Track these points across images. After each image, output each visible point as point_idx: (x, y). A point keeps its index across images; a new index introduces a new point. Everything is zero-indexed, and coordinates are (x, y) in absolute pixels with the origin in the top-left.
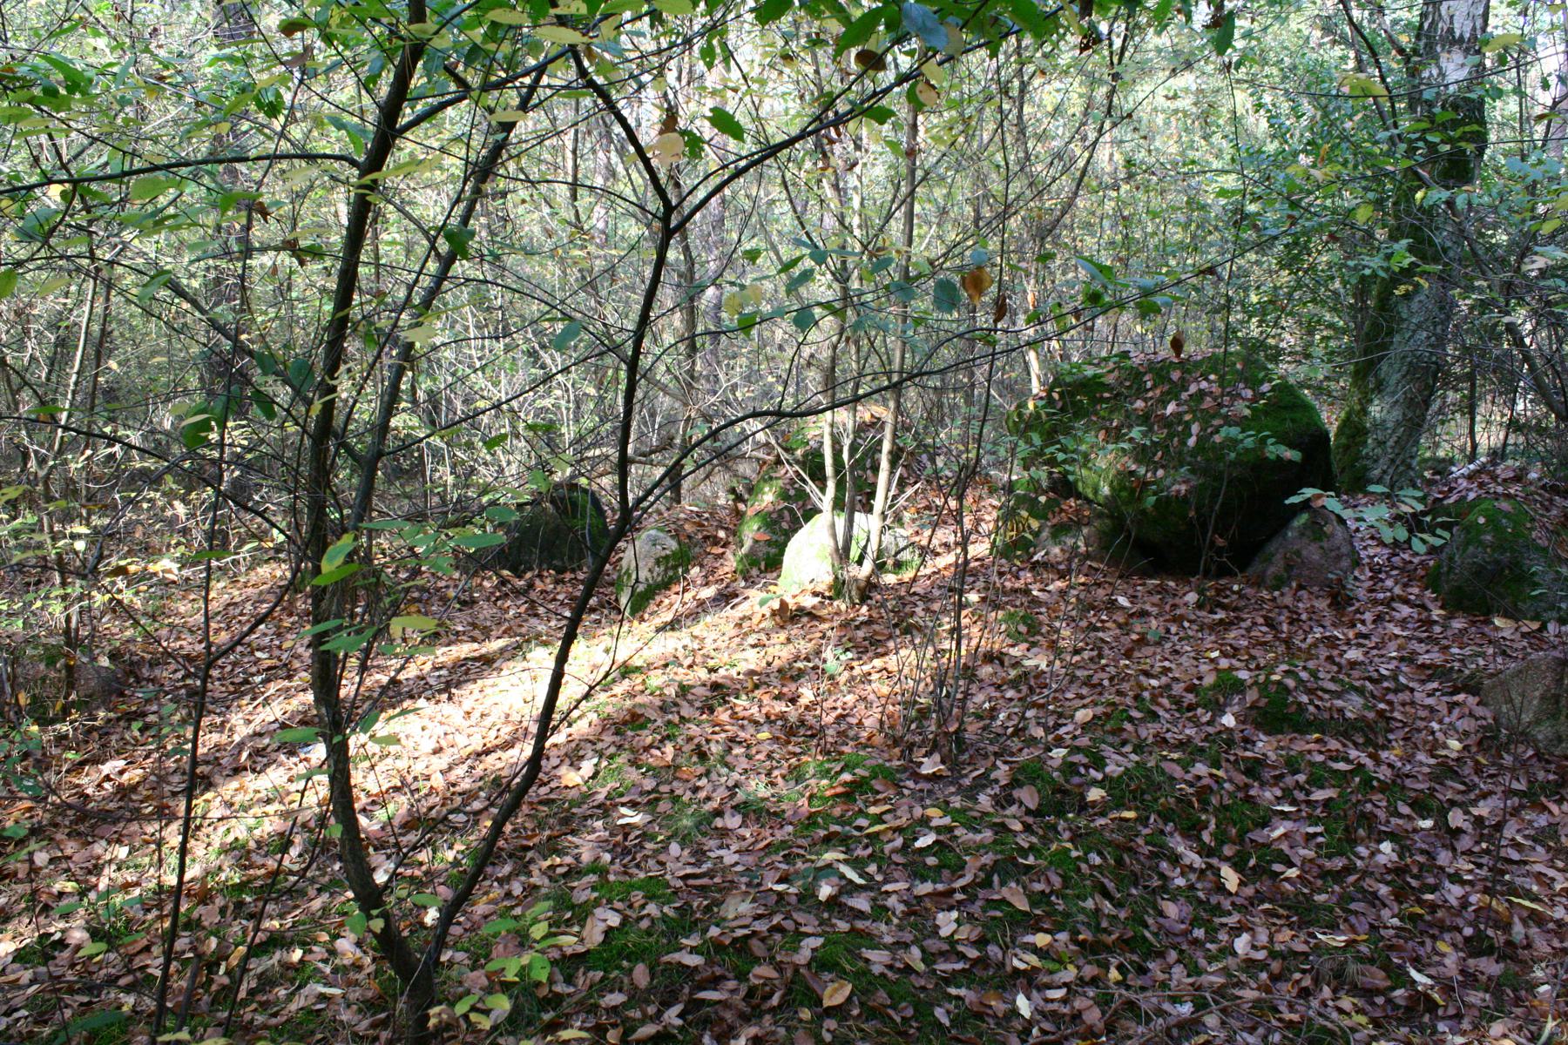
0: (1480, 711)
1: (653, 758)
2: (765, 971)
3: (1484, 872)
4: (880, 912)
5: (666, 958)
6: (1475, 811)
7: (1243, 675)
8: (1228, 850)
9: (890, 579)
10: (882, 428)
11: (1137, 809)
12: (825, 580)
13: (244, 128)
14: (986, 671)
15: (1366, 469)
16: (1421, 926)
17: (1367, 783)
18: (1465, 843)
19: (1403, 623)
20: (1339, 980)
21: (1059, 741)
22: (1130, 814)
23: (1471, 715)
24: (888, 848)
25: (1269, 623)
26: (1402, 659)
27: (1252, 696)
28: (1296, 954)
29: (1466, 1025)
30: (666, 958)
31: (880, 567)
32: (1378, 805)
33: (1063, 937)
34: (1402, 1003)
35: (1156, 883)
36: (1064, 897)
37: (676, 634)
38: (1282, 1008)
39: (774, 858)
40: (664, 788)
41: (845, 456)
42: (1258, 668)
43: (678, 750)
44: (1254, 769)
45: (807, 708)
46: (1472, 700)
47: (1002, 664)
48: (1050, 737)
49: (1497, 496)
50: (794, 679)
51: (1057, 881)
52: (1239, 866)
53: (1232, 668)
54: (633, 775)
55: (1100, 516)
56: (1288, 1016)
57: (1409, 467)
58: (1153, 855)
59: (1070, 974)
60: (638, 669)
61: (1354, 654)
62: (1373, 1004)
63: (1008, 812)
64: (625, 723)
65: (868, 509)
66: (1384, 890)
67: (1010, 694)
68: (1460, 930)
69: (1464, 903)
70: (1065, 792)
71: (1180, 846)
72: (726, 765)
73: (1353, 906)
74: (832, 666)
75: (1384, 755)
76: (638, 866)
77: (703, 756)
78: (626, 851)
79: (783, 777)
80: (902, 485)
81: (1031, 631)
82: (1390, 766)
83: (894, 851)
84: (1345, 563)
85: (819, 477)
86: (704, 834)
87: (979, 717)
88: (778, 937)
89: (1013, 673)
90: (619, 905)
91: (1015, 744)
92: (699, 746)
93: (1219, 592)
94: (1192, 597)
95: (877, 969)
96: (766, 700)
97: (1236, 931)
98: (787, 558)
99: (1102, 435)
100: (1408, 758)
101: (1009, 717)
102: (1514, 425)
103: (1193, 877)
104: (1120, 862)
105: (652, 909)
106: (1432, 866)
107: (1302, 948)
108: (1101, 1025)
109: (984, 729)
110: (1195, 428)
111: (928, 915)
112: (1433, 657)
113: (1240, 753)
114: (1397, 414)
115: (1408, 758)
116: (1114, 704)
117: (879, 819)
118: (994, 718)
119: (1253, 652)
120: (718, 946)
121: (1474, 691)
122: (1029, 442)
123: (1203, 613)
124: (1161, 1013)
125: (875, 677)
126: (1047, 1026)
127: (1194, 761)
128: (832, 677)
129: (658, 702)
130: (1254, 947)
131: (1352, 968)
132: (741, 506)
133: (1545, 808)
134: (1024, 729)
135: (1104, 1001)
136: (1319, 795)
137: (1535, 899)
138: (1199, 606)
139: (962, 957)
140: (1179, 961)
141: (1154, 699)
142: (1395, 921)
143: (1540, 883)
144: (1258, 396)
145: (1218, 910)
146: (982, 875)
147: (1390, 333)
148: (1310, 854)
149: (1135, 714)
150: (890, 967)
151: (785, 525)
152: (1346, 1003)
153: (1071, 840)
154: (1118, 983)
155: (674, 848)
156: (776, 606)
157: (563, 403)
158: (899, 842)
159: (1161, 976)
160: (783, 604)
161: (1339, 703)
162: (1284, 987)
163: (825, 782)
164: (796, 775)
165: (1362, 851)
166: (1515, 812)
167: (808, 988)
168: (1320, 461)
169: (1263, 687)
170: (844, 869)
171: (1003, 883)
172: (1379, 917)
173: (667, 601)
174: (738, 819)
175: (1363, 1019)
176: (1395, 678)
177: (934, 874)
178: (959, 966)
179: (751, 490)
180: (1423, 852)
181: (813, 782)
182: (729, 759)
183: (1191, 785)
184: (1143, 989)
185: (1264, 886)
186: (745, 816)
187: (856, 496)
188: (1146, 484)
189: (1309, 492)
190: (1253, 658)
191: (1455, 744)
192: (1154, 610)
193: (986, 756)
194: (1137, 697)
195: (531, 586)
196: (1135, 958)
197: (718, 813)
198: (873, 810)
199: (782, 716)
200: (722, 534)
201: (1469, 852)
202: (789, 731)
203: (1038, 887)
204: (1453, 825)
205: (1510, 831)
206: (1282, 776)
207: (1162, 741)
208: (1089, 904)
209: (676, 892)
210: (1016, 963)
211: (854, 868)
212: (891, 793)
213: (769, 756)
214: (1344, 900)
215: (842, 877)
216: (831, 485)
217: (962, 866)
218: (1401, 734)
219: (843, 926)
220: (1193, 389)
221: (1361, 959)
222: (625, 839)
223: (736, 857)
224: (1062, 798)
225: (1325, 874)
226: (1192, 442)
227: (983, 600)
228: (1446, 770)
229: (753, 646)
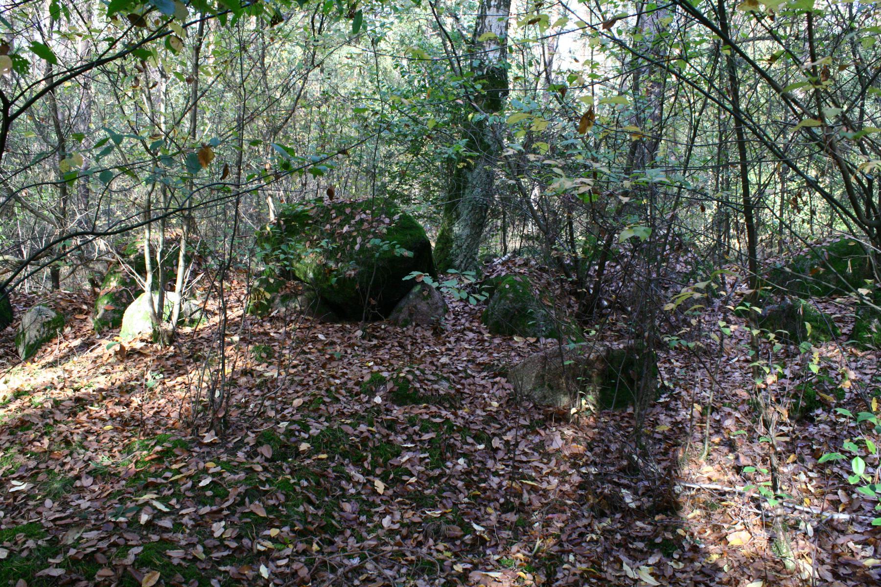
0: (507, 386)
1: (36, 447)
2: (106, 572)
3: (509, 469)
4: (178, 526)
5: (40, 573)
6: (505, 438)
7: (385, 374)
8: (378, 471)
9: (188, 330)
10: (179, 242)
11: (327, 453)
12: (148, 332)
14: (243, 380)
15: (452, 261)
16: (479, 500)
17: (451, 428)
18: (500, 455)
19: (470, 342)
20: (438, 535)
21: (284, 418)
22: (324, 456)
23: (503, 388)
24: (183, 488)
25: (401, 345)
26: (469, 361)
27: (390, 385)
28: (415, 523)
29: (500, 549)
30: (40, 573)
31: (181, 323)
32: (456, 440)
33: (286, 529)
34: (469, 542)
35: (339, 493)
36: (286, 506)
37: (54, 369)
38: (408, 554)
39: (113, 501)
40: (43, 466)
41: (158, 258)
42: (393, 370)
43: (52, 441)
44: (391, 425)
45: (136, 409)
46: (503, 380)
47: (252, 376)
48: (278, 416)
49: (516, 274)
50: (128, 392)
51: (282, 498)
52: (384, 479)
53: (380, 371)
54: (21, 459)
55: (308, 289)
56: (411, 558)
57: (474, 259)
58: (337, 478)
59: (288, 551)
60: (27, 393)
61: (444, 360)
62: (455, 545)
63: (255, 460)
64: (17, 427)
65: (173, 289)
66: (460, 484)
67: (257, 393)
68: (498, 500)
69: (500, 486)
70: (287, 447)
71: (353, 471)
72: (84, 447)
73: (445, 494)
74: (151, 382)
75: (460, 412)
76: (23, 517)
77: (67, 443)
78: (15, 508)
79: (120, 451)
80: (194, 274)
81: (269, 355)
82: (463, 418)
83: (187, 490)
84: (441, 311)
85: (142, 271)
86: (69, 492)
87: (238, 407)
88: (114, 550)
89: (258, 381)
90: (7, 544)
91: (259, 421)
92: (66, 437)
93: (374, 329)
94: (359, 333)
95: (175, 562)
96: (110, 406)
97: (383, 515)
98: (124, 320)
99: (308, 244)
100: (472, 413)
101: (255, 406)
102: (528, 238)
103: (359, 488)
104: (318, 484)
105: (31, 543)
106: (484, 469)
107: (418, 520)
108: (308, 577)
109: (241, 414)
110: (359, 240)
111: (208, 525)
112: (483, 359)
113: (384, 417)
114: (467, 231)
115: (472, 413)
116: (315, 395)
117: (178, 471)
118: (247, 407)
119: (392, 361)
120: (74, 561)
121: (503, 374)
122: (264, 249)
123: (365, 342)
124: (341, 565)
125: (178, 387)
126: (277, 581)
127: (359, 424)
128: (151, 389)
129: (39, 412)
130: (393, 523)
131: (444, 527)
132: (97, 290)
133: (538, 433)
134: (264, 412)
135: (309, 564)
136: (426, 437)
137: (534, 480)
138: (363, 337)
139: (227, 547)
140: (351, 535)
141: (337, 391)
142: (466, 500)
143: (536, 471)
144: (392, 221)
145: (374, 505)
146: (239, 498)
147: (465, 188)
148: (422, 469)
149: (327, 400)
150: (184, 559)
151: (124, 300)
152: (441, 547)
153: (291, 474)
154: (317, 552)
155: (48, 503)
156: (118, 349)
158: (190, 484)
159: (342, 545)
160: (122, 347)
161: (436, 386)
162: (409, 542)
163: (145, 452)
164: (128, 449)
165: (449, 464)
166: (524, 437)
167: (133, 579)
168: (423, 257)
169: (395, 380)
170: (155, 503)
171: (251, 502)
172: (458, 499)
173: (49, 349)
174: (90, 480)
175: (449, 554)
176: (465, 371)
177: (211, 500)
178: (225, 553)
179: (104, 279)
180: (479, 462)
181: (138, 453)
182: (85, 443)
183: (357, 437)
184: (332, 553)
185: (398, 488)
186: (95, 478)
187: (165, 281)
188: (331, 271)
189: (415, 274)
190: (392, 364)
191: (495, 404)
192: (339, 341)
193: (242, 430)
194: (328, 390)
196: (327, 536)
197: (78, 477)
198: (174, 467)
199: (120, 415)
200: (85, 307)
201: (502, 460)
202: (123, 423)
203: (271, 502)
204: (494, 446)
205: (521, 447)
206: (406, 428)
207: (341, 414)
208: (301, 509)
209: (48, 530)
210: (259, 547)
211: (162, 503)
212: (185, 455)
213: (111, 440)
214: (440, 491)
215: (155, 508)
216: (149, 276)
217: (227, 494)
218: (468, 400)
219: (155, 538)
220: (357, 218)
221: (448, 522)
222: (15, 500)
223: (89, 504)
224: (286, 450)
225: (430, 479)
226: (357, 247)
227: (241, 339)
228: (491, 418)
229: (103, 374)
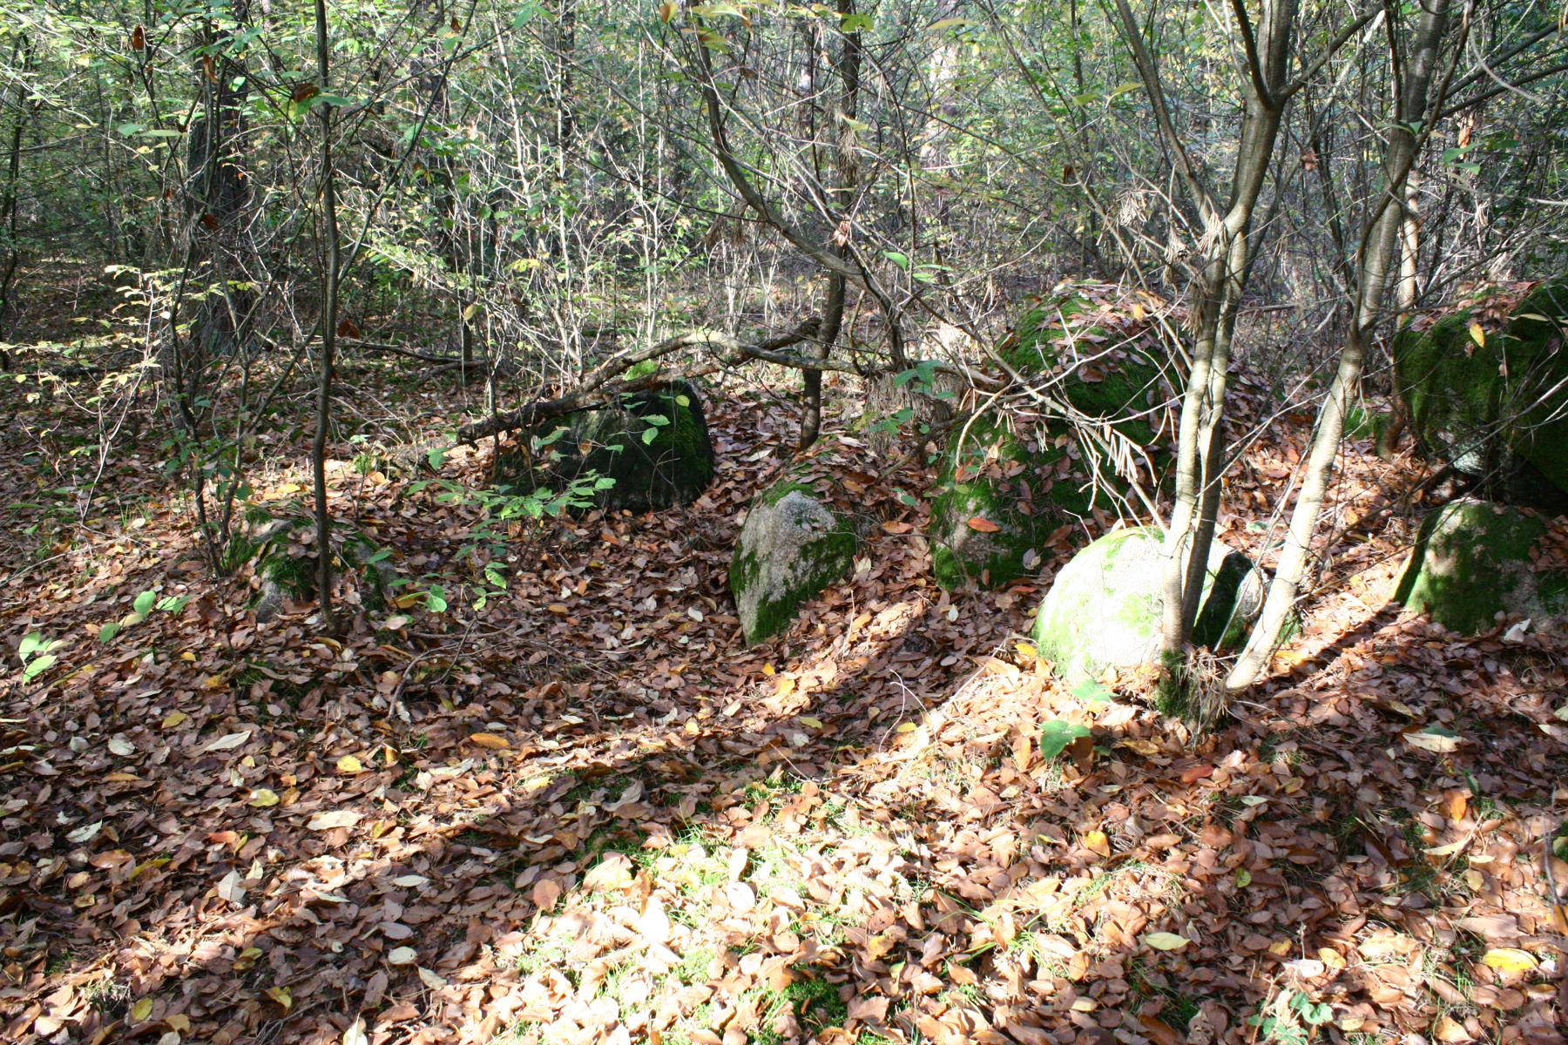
157: (646, 238)
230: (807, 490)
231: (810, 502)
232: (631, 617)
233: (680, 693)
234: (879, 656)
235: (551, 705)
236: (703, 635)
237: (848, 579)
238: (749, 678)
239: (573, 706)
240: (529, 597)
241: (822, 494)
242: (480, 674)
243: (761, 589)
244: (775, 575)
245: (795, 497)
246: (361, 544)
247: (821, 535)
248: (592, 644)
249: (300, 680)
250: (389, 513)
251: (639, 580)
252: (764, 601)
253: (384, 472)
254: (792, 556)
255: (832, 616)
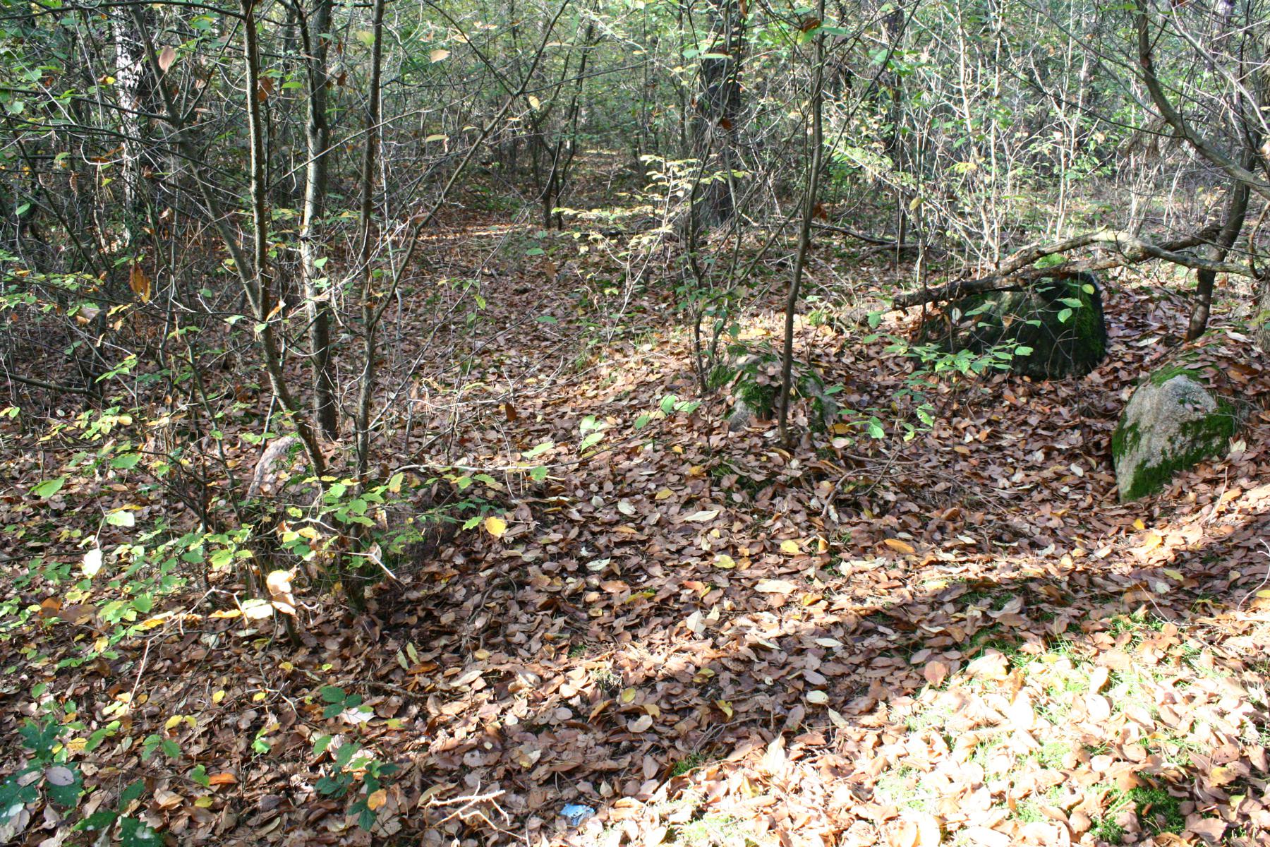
13: (254, 778)
157: (1062, 149)
195: (998, 397)
230: (1193, 375)
231: (1194, 385)
232: (1022, 465)
233: (1059, 532)
234: (1245, 528)
235: (950, 526)
236: (1083, 488)
237: (1222, 458)
238: (1120, 529)
239: (968, 529)
240: (939, 438)
241: (1207, 380)
242: (896, 493)
243: (1139, 457)
244: (1156, 444)
245: (1181, 380)
246: (812, 380)
247: (1200, 415)
248: (987, 482)
249: (759, 478)
250: (833, 359)
251: (1031, 436)
252: (1141, 466)
253: (831, 325)
254: (1172, 430)
255: (1202, 487)
